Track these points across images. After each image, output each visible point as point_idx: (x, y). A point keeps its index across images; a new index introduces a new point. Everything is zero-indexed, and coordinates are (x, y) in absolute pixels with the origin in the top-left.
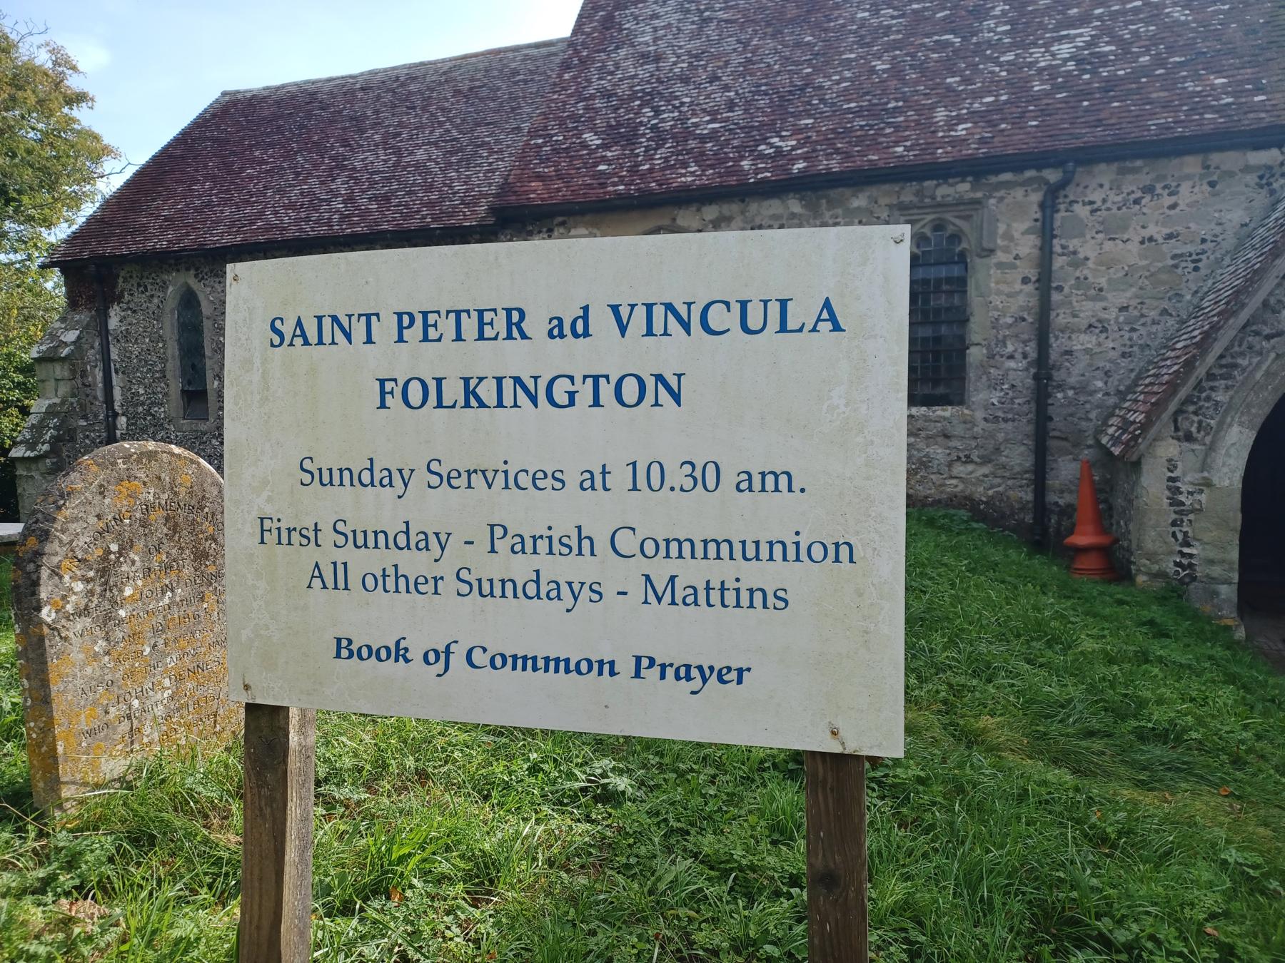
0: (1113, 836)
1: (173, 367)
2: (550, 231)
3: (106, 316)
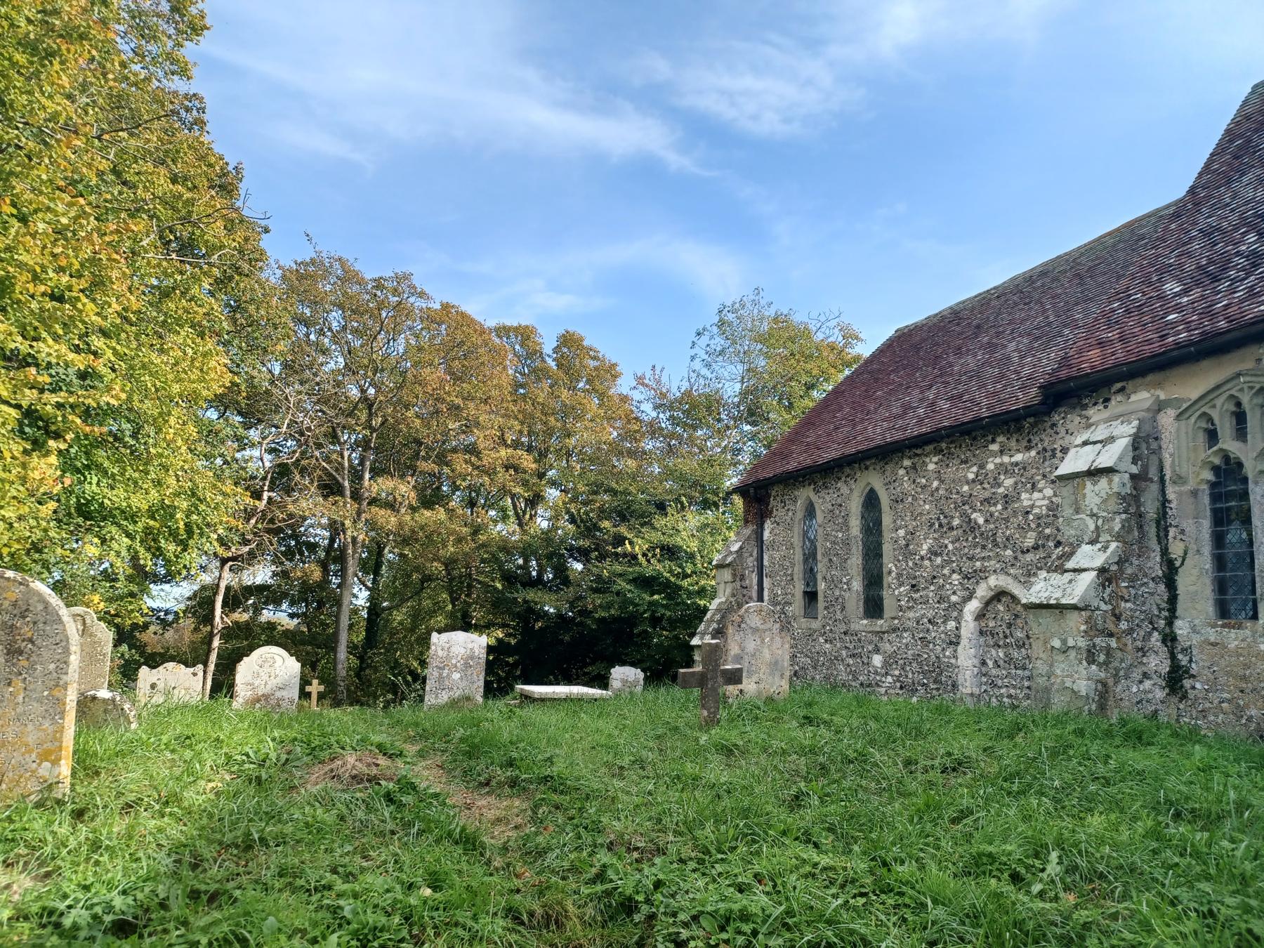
0: (1002, 477)
1: (798, 570)
2: (1107, 400)
3: (762, 529)
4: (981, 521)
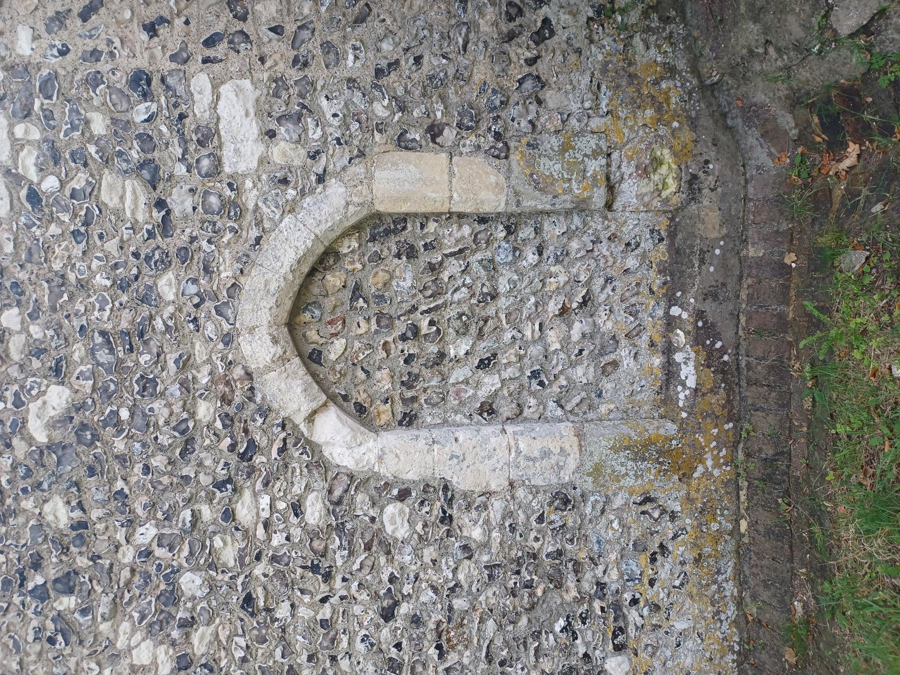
4: (57, 398)
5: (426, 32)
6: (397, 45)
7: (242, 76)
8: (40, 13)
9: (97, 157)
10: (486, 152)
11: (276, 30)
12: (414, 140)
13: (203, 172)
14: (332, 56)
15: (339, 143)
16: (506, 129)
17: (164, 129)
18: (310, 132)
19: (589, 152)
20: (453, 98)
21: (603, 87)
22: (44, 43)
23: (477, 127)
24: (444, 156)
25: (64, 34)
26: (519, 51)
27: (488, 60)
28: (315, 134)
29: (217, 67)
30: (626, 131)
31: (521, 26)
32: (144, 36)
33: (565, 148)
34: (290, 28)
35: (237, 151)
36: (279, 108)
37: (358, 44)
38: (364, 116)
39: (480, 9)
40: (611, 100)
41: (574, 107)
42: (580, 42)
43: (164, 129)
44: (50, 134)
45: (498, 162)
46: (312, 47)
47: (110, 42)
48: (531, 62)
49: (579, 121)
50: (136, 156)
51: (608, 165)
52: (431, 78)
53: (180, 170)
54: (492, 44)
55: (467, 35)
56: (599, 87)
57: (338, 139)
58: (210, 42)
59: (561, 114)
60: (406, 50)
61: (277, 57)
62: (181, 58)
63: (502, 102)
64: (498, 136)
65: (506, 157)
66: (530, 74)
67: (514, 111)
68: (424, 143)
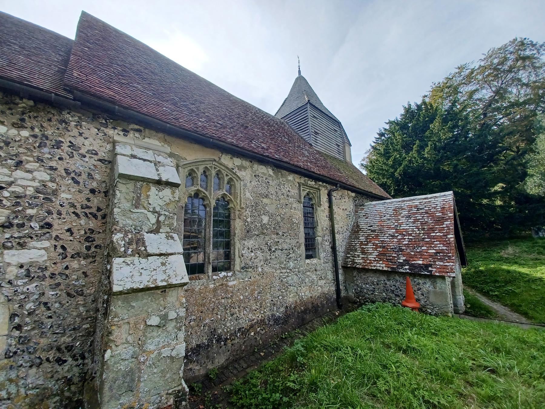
5: (62, 318)
6: (57, 309)
7: (48, 257)
8: (76, 201)
9: (16, 209)
10: (8, 349)
11: (67, 268)
12: (14, 320)
13: (6, 244)
14: (54, 286)
15: (15, 291)
16: (19, 355)
17: (27, 231)
18: (21, 281)
19: (9, 390)
20: (33, 333)
21: (38, 390)
22: (65, 201)
23: (19, 344)
24: (6, 333)
25: (68, 207)
26: (52, 354)
27: (49, 343)
28: (20, 282)
29: (53, 249)
30: (19, 403)
31: (64, 352)
32: (66, 228)
33: (11, 381)
34: (67, 272)
35: (14, 255)
36: (32, 270)
37: (58, 295)
38: (27, 300)
39: (71, 336)
40: (32, 394)
41: (29, 381)
42: (56, 376)
43: (27, 231)
44: (28, 197)
45: (4, 354)
46: (59, 279)
47: (64, 219)
48: (48, 360)
49: (23, 384)
50: (15, 222)
51: (4, 399)
52: (42, 323)
53: (7, 236)
54: (55, 343)
55: (60, 333)
56: (37, 388)
57: (17, 291)
58: (63, 247)
59: (26, 376)
60: (55, 312)
61: (56, 268)
62: (57, 238)
63: (30, 352)
64: (15, 353)
65: (6, 358)
66: (42, 361)
67: (26, 357)
68: (13, 324)
